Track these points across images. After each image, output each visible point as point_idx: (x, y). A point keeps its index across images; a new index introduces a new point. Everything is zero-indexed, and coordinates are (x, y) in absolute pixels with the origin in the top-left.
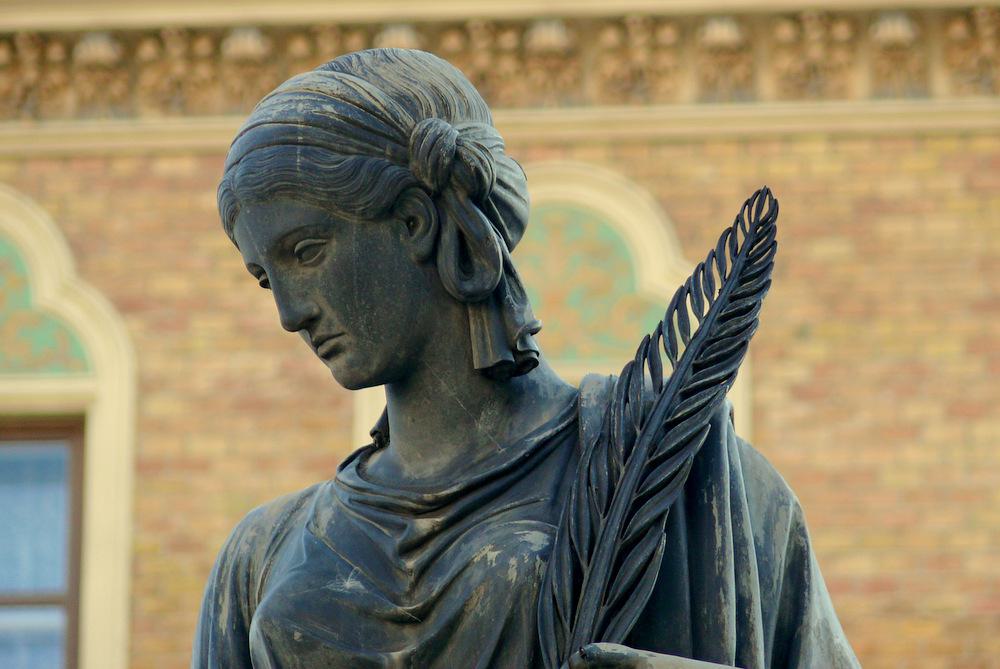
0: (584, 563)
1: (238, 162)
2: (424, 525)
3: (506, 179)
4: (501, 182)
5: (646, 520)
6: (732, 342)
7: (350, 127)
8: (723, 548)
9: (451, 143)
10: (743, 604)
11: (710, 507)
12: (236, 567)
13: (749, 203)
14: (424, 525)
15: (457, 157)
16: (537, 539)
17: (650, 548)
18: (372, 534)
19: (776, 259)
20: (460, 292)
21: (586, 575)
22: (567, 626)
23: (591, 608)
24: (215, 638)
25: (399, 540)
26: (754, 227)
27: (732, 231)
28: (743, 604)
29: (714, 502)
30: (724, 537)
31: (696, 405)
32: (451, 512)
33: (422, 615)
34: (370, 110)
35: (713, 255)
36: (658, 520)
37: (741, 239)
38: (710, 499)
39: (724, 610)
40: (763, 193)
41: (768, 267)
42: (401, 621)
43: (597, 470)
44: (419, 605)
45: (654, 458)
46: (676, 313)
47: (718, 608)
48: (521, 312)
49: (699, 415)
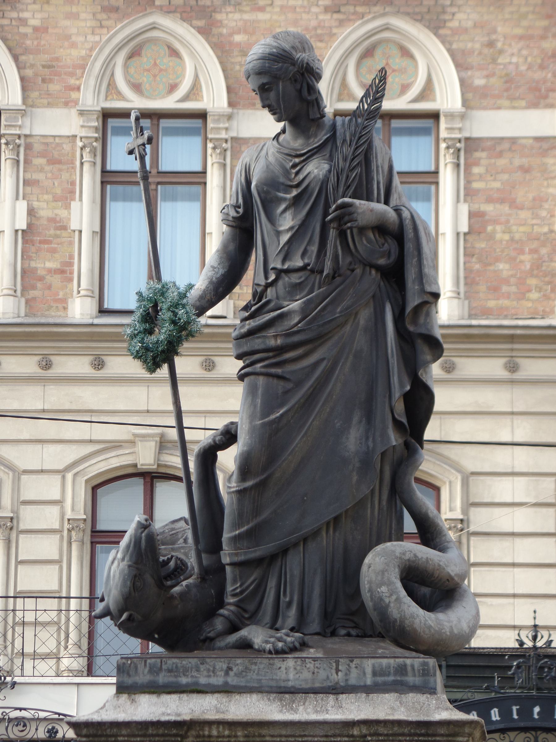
0: (340, 175)
1: (250, 62)
2: (297, 160)
3: (318, 67)
4: (317, 68)
5: (355, 163)
6: (375, 113)
7: (280, 56)
8: (374, 169)
9: (306, 61)
10: (378, 183)
11: (370, 158)
12: (246, 165)
13: (379, 71)
14: (297, 160)
15: (307, 64)
16: (326, 167)
17: (356, 171)
18: (283, 162)
19: (387, 87)
20: (370, 590)
21: (340, 178)
22: (336, 192)
23: (341, 190)
24: (241, 184)
25: (291, 164)
26: (381, 77)
27: (375, 79)
28: (378, 183)
29: (371, 156)
30: (374, 167)
31: (367, 131)
32: (305, 157)
33: (298, 186)
34: (284, 51)
35: (370, 86)
36: (358, 164)
37: (377, 81)
38: (370, 155)
39: (372, 173)
40: (383, 69)
41: (384, 89)
42: (292, 187)
43: (343, 149)
44: (296, 183)
45: (357, 145)
46: (361, 104)
47: (372, 186)
48: (322, 103)
49: (368, 133)
